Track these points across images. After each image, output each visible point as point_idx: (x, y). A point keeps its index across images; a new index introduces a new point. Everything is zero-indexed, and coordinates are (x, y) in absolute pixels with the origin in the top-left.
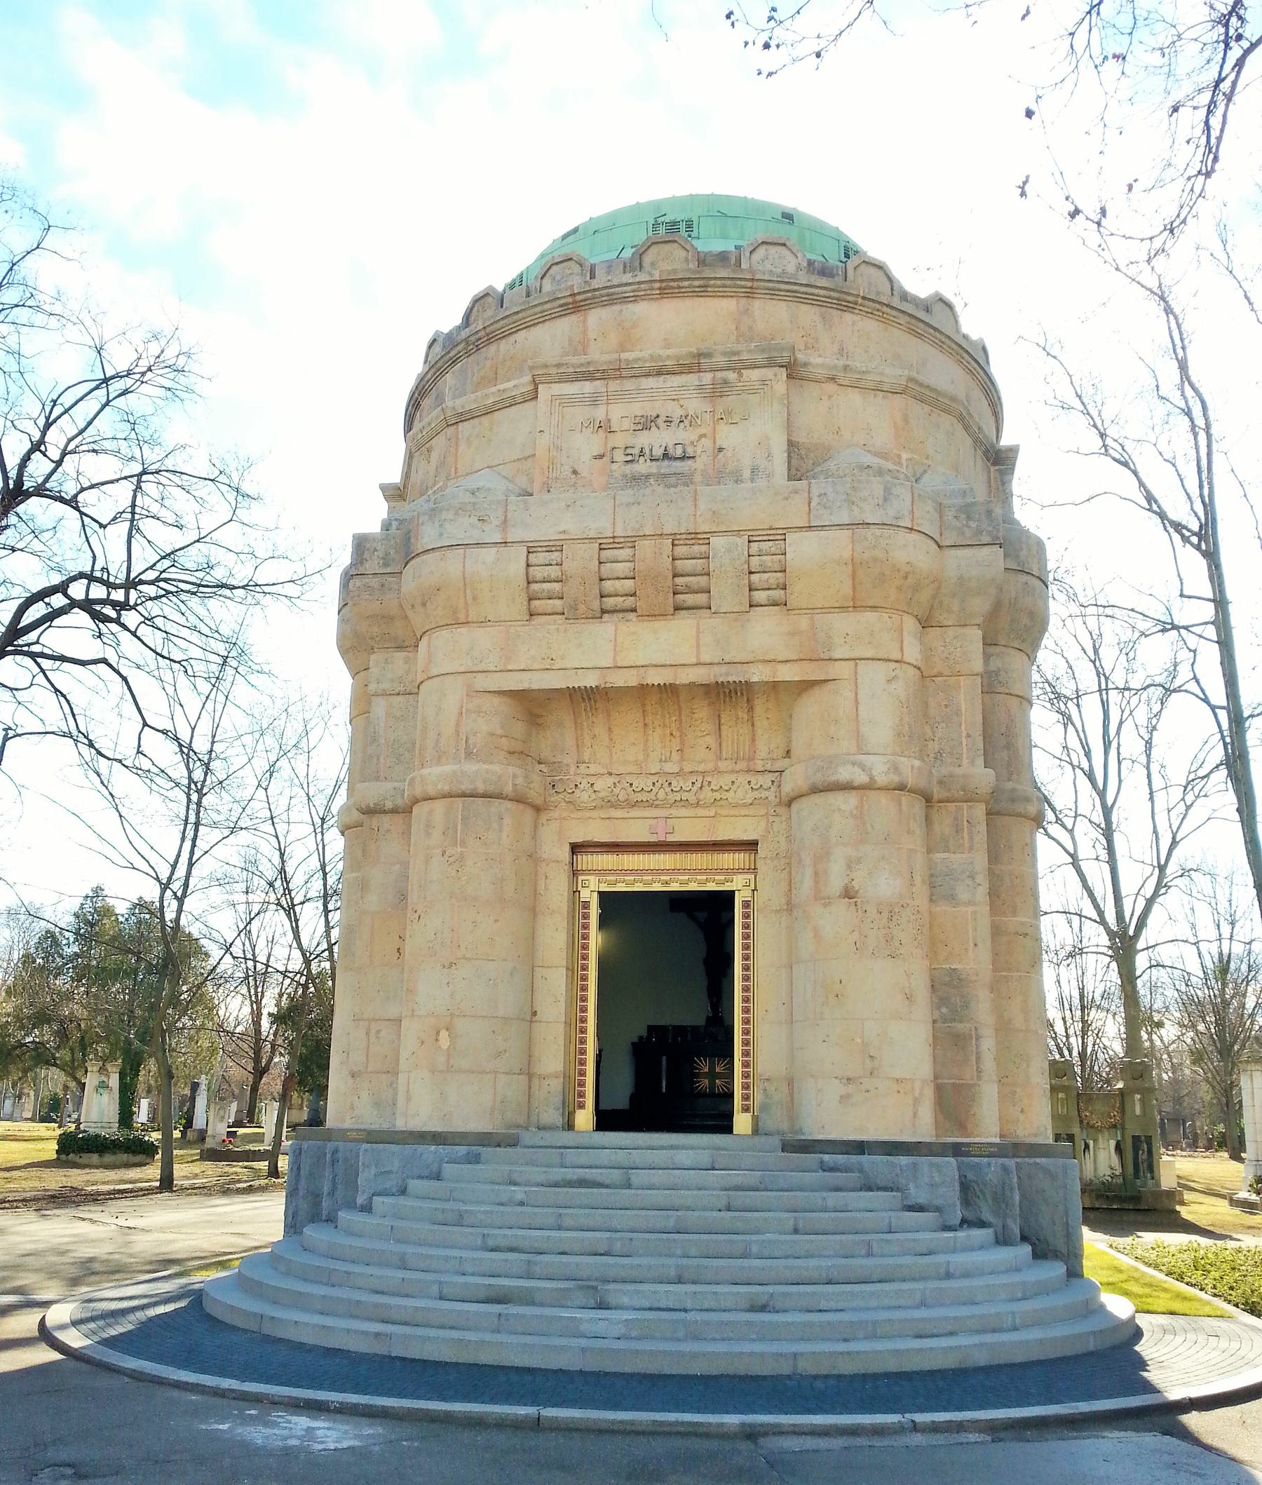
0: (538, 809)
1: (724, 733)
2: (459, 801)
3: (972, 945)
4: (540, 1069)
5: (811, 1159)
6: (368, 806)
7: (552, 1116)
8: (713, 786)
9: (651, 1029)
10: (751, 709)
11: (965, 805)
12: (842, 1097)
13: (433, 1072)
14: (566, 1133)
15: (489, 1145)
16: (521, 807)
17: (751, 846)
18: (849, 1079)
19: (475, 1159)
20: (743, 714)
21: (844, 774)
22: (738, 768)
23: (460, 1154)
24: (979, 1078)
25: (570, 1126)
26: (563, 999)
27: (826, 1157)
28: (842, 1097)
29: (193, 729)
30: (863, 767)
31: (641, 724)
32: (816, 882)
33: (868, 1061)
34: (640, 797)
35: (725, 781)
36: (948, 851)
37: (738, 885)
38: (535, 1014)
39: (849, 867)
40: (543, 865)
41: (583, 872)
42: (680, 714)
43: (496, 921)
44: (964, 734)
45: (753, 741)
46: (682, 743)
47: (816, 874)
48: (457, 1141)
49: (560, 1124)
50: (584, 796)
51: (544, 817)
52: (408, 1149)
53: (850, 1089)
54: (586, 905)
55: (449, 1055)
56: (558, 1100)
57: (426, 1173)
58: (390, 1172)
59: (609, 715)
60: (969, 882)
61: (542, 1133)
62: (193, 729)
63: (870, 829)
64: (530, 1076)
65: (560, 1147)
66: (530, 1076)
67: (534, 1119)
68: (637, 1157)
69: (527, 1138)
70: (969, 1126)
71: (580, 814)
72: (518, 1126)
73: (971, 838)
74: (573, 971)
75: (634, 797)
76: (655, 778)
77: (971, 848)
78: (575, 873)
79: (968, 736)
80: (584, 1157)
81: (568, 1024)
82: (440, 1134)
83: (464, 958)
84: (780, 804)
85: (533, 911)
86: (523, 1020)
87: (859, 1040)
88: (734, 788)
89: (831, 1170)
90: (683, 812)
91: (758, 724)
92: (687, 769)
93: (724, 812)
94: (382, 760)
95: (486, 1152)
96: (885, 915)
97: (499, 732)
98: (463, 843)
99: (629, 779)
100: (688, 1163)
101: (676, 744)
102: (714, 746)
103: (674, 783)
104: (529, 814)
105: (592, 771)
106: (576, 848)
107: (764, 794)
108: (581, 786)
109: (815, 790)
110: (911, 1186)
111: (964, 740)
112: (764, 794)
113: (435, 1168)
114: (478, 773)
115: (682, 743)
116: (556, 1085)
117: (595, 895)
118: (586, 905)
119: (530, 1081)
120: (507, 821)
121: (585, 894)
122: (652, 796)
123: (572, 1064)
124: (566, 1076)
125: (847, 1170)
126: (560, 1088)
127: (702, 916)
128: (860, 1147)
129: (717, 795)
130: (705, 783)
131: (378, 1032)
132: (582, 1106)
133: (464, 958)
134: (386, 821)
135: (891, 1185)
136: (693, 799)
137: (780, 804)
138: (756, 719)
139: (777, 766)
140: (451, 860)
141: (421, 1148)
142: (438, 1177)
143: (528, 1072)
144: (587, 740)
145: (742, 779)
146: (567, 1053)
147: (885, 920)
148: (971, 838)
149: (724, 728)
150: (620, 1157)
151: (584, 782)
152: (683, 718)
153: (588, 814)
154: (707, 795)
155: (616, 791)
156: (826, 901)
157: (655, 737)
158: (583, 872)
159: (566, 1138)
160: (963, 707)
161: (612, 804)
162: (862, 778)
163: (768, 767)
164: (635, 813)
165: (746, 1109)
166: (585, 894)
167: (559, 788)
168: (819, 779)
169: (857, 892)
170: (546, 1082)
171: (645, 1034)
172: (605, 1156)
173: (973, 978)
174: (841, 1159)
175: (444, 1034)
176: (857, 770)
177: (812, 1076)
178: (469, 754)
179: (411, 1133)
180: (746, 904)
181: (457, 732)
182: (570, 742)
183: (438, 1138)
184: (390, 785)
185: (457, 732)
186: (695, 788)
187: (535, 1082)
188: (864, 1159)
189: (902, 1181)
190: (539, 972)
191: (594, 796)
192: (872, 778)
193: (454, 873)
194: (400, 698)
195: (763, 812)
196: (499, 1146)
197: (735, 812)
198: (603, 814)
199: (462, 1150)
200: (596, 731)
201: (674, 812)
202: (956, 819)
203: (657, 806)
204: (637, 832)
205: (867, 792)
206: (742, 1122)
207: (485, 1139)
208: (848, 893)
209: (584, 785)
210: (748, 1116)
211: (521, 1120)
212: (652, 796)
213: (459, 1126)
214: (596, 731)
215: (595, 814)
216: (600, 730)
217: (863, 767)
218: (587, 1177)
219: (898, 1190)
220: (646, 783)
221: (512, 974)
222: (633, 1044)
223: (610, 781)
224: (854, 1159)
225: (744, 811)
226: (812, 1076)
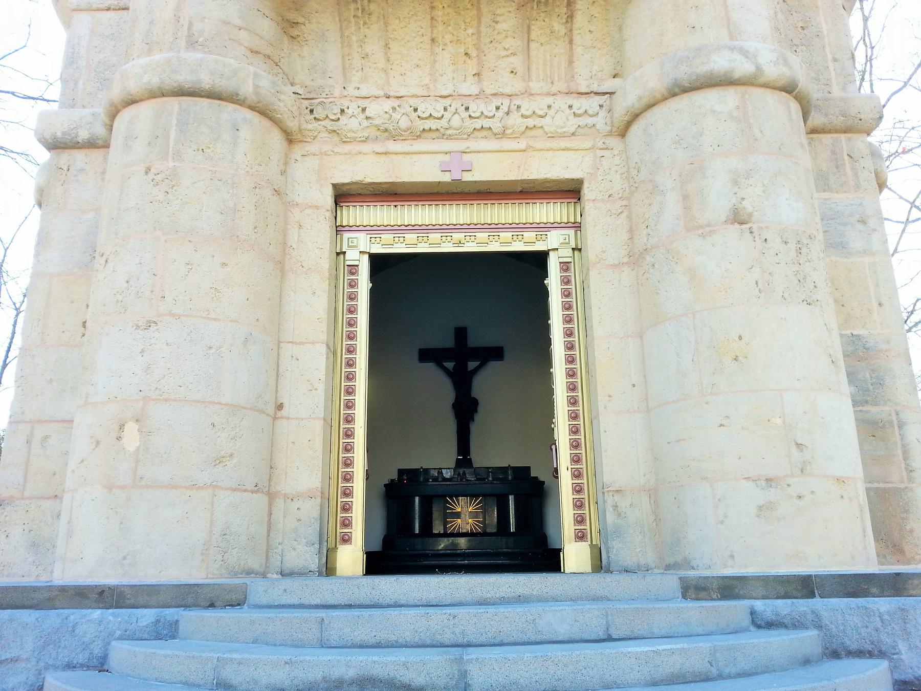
0: (290, 138)
1: (533, 53)
2: (174, 103)
3: (875, 304)
4: (285, 486)
5: (736, 610)
6: (55, 138)
7: (306, 556)
8: (523, 111)
9: (401, 472)
10: (570, 18)
11: (842, 136)
12: (760, 508)
13: (110, 488)
14: (325, 582)
15: (196, 605)
16: (266, 123)
17: (571, 191)
18: (768, 480)
19: (167, 632)
20: (559, 27)
21: (720, 63)
22: (554, 89)
23: (143, 623)
24: (910, 480)
25: (328, 569)
26: (321, 387)
27: (759, 605)
28: (760, 508)
29: (6, 250)
30: (744, 52)
31: (427, 39)
32: (687, 208)
33: (794, 451)
34: (428, 124)
35: (538, 105)
36: (830, 190)
37: (554, 242)
38: (280, 407)
39: (736, 183)
40: (296, 211)
41: (350, 229)
42: (479, 22)
43: (224, 265)
44: (830, 57)
45: (571, 62)
46: (481, 64)
47: (686, 197)
48: (141, 600)
49: (314, 566)
50: (351, 124)
51: (298, 151)
52: (53, 617)
53: (772, 494)
54: (353, 269)
55: (137, 461)
56: (312, 532)
57: (81, 658)
58: (16, 660)
59: (386, 25)
60: (860, 226)
61: (287, 583)
62: (6, 250)
63: (758, 135)
64: (272, 497)
65: (317, 607)
66: (272, 497)
67: (275, 561)
68: (469, 622)
69: (259, 591)
70: (907, 548)
71: (347, 148)
72: (249, 572)
73: (856, 175)
74: (335, 353)
75: (420, 125)
76: (447, 102)
77: (857, 186)
78: (339, 230)
79: (835, 60)
80: (365, 626)
81: (328, 423)
82: (112, 589)
83: (171, 314)
84: (610, 134)
85: (280, 265)
86: (261, 411)
87: (778, 421)
88: (551, 112)
89: (770, 625)
90: (484, 145)
91: (577, 39)
92: (489, 91)
93: (538, 145)
94: (80, 85)
95: (189, 618)
96: (793, 246)
97: (238, 22)
98: (178, 155)
99: (412, 102)
100: (563, 630)
101: (472, 66)
102: (520, 70)
103: (473, 107)
104: (276, 138)
105: (363, 92)
106: (343, 195)
107: (590, 121)
108: (350, 112)
109: (679, 90)
110: (902, 647)
111: (831, 66)
112: (590, 121)
113: (97, 650)
114: (200, 68)
115: (481, 64)
116: (310, 509)
117: (366, 257)
118: (353, 269)
119: (270, 505)
120: (244, 133)
121: (352, 256)
122: (443, 123)
123: (333, 482)
124: (325, 498)
125: (796, 625)
126: (316, 513)
127: (450, 365)
128: (806, 586)
129: (530, 122)
130: (513, 108)
131: (46, 438)
132: (346, 540)
133: (171, 314)
134: (80, 156)
135: (869, 647)
136: (496, 125)
137: (610, 134)
138: (575, 32)
139: (608, 86)
140: (159, 177)
141: (75, 615)
142: (101, 665)
143: (267, 489)
144: (357, 61)
145: (561, 103)
146: (326, 465)
147: (793, 254)
148: (856, 175)
149: (533, 45)
150: (437, 623)
151: (353, 106)
152: (483, 29)
153: (357, 147)
154: (516, 121)
155: (396, 116)
156: (705, 230)
157: (445, 57)
158: (350, 229)
159: (325, 590)
160: (825, 28)
161: (393, 134)
162: (743, 68)
163: (595, 88)
164: (419, 146)
165: (580, 537)
166: (352, 256)
167: (319, 112)
168: (684, 73)
169: (750, 215)
170: (296, 504)
171: (395, 476)
172: (406, 624)
173: (884, 347)
174: (783, 607)
175: (131, 428)
176: (736, 56)
177: (705, 479)
178: (192, 44)
179: (63, 589)
180: (565, 267)
181: (177, 19)
182: (333, 60)
183: (107, 597)
184: (86, 111)
185: (177, 19)
186: (500, 114)
187: (279, 504)
188: (817, 603)
189: (886, 639)
190: (287, 351)
191: (366, 123)
192: (758, 68)
193: (161, 196)
194: (111, 14)
195: (588, 144)
196: (212, 605)
197: (550, 144)
198: (379, 148)
199: (146, 616)
200: (369, 48)
201: (472, 145)
202: (834, 153)
203: (450, 138)
204: (424, 169)
205: (751, 89)
206: (575, 556)
207: (190, 596)
208: (738, 218)
209: (353, 109)
210: (584, 547)
211: (255, 563)
212: (443, 123)
213: (148, 573)
214: (369, 48)
215: (367, 148)
216: (374, 47)
217: (744, 52)
218: (378, 671)
219: (882, 654)
220: (435, 107)
221: (246, 341)
222: (385, 485)
223: (387, 105)
224: (803, 606)
225: (564, 143)
226: (705, 479)
